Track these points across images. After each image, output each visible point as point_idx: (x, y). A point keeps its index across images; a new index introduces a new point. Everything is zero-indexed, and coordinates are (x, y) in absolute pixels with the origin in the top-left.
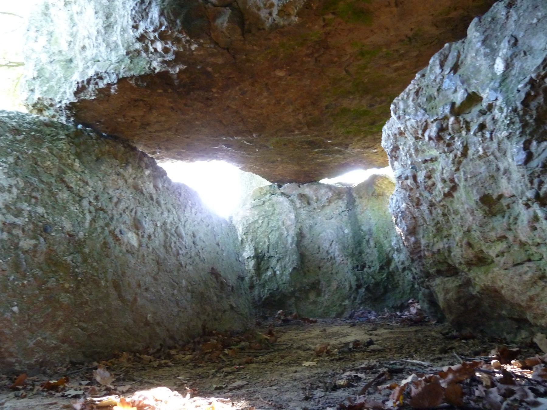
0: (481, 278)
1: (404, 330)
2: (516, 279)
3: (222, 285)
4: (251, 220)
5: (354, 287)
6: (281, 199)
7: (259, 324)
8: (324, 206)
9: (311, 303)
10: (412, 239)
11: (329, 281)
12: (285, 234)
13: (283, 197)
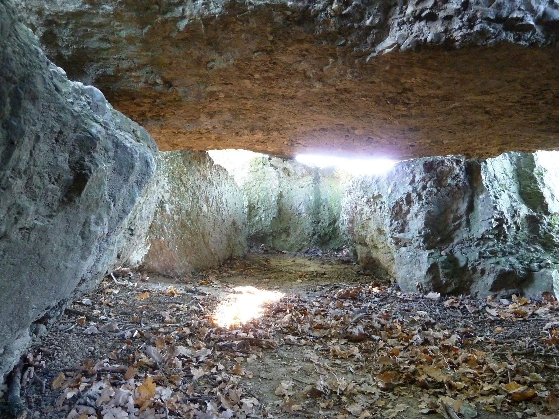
0: (375, 254)
1: (339, 266)
2: (385, 258)
4: (248, 181)
6: (271, 169)
7: (249, 252)
8: (298, 178)
9: (283, 241)
10: (351, 225)
11: (296, 229)
12: (271, 194)
13: (272, 168)
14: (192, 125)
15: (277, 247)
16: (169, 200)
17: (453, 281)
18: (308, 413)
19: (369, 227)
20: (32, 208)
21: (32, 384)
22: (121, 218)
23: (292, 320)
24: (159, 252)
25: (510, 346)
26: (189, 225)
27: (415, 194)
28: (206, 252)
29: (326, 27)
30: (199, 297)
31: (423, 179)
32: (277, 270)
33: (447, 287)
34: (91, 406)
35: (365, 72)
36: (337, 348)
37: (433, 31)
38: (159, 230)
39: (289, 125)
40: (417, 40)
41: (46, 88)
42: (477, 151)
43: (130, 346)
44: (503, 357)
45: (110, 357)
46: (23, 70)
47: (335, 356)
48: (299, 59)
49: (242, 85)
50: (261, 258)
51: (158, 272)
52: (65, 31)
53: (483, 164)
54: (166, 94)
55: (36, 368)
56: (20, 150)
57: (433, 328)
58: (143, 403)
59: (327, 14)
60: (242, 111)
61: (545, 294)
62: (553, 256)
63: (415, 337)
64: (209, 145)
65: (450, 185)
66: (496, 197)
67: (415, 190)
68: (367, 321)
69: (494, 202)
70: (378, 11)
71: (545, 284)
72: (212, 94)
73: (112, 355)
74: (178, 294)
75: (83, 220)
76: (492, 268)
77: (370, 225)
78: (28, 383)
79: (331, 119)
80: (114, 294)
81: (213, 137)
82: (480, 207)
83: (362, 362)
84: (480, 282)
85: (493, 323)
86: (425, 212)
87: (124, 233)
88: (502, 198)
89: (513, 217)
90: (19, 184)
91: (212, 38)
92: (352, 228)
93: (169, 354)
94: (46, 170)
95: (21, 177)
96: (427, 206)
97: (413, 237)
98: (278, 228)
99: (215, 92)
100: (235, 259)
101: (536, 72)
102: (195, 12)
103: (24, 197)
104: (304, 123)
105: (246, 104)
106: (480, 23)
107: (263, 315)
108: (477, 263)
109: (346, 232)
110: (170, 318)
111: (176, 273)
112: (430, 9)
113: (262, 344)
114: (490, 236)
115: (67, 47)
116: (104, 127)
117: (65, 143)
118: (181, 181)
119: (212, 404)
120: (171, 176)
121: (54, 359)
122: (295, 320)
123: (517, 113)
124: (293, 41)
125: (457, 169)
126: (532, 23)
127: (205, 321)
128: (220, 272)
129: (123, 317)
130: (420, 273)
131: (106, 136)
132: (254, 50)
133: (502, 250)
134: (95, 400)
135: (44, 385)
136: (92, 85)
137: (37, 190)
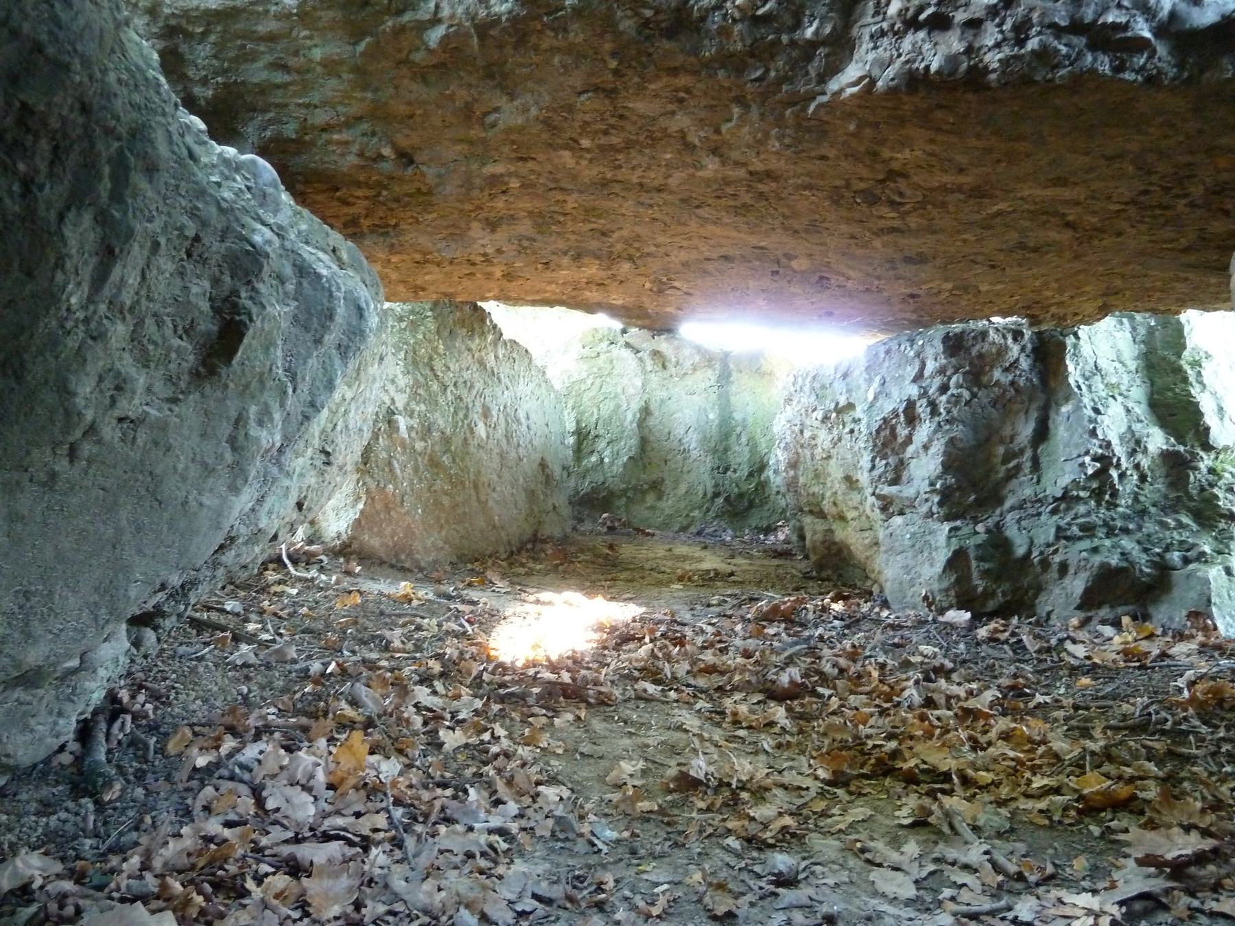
0: (840, 534)
1: (766, 562)
3: (548, 479)
4: (576, 377)
5: (709, 495)
6: (627, 353)
7: (574, 529)
8: (686, 374)
9: (648, 508)
10: (792, 473)
11: (677, 482)
12: (624, 407)
13: (629, 350)
14: (453, 246)
15: (636, 522)
16: (405, 409)
17: (999, 587)
18: (669, 816)
19: (829, 475)
20: (141, 381)
21: (129, 746)
22: (307, 418)
23: (653, 655)
24: (382, 516)
25: (1103, 713)
26: (448, 464)
27: (924, 402)
28: (481, 523)
29: (724, 42)
30: (461, 607)
31: (942, 371)
32: (632, 566)
33: (986, 599)
34: (241, 781)
35: (807, 137)
36: (743, 709)
37: (942, 50)
38: (383, 470)
39: (653, 249)
40: (910, 69)
41: (174, 152)
42: (1053, 310)
43: (319, 688)
44: (1086, 733)
45: (280, 706)
46: (134, 115)
47: (736, 723)
48: (670, 107)
49: (556, 161)
50: (600, 543)
51: (380, 558)
52: (200, 47)
53: (1070, 340)
54: (401, 180)
55: (135, 718)
56: (124, 267)
57: (948, 679)
58: (342, 780)
59: (726, 15)
60: (555, 216)
61: (1194, 615)
62: (1216, 538)
63: (906, 693)
64: (489, 291)
65: (997, 383)
66: (1097, 411)
67: (924, 394)
68: (809, 660)
69: (1090, 421)
70: (831, 10)
71: (1193, 595)
72: (494, 180)
73: (283, 703)
74: (419, 599)
75: (234, 414)
76: (1083, 561)
77: (830, 470)
78: (119, 742)
79: (742, 235)
80: (289, 596)
81: (498, 274)
82: (1061, 431)
83: (792, 735)
84: (1057, 591)
85: (1074, 671)
86: (943, 441)
87: (312, 459)
88: (1110, 412)
89: (1132, 453)
90: (119, 331)
91: (494, 64)
92: (795, 478)
93: (397, 700)
94: (169, 310)
95: (124, 319)
96: (948, 427)
97: (918, 493)
98: (638, 480)
99: (502, 175)
100: (544, 541)
101: (1165, 137)
102: (460, 10)
103: (128, 359)
104: (685, 243)
105: (565, 201)
106: (1039, 33)
107: (595, 645)
108: (1052, 549)
109: (783, 490)
110: (403, 642)
111: (418, 561)
112: (936, 5)
113: (588, 695)
114: (1082, 494)
115: (204, 82)
116: (278, 235)
117: (205, 261)
118: (432, 369)
119: (479, 793)
120: (410, 359)
121: (170, 705)
122: (660, 655)
123: (1133, 227)
124: (659, 70)
125: (1015, 349)
126: (1147, 34)
127: (474, 649)
128: (511, 564)
129: (307, 637)
130: (931, 571)
131: (281, 252)
132: (579, 89)
133: (1106, 524)
134: (251, 771)
135: (152, 747)
136: (257, 154)
137: (151, 347)
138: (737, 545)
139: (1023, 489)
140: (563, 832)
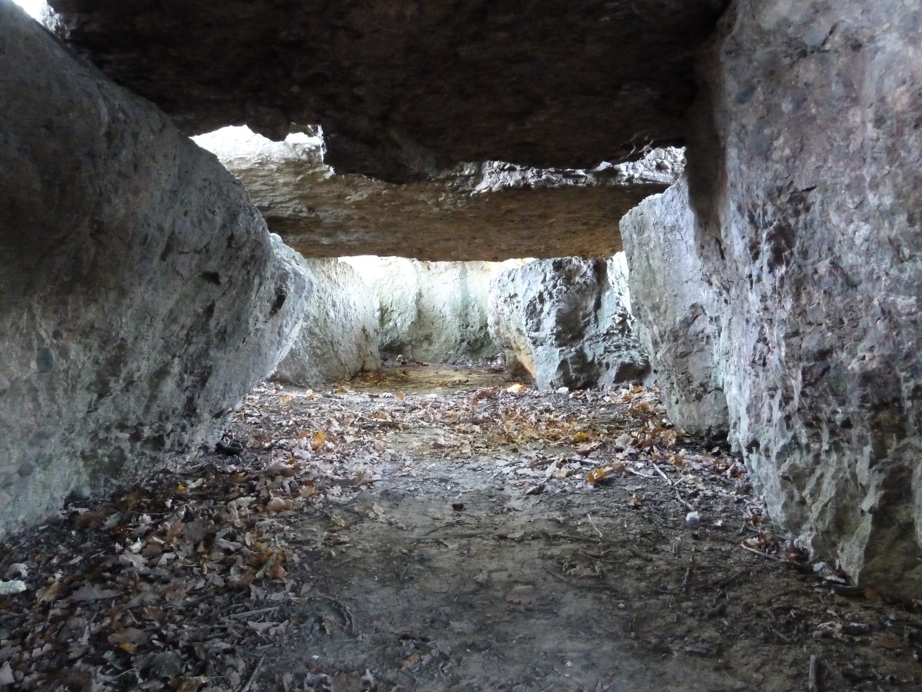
7: (383, 364)
11: (439, 335)
27: (546, 293)
31: (553, 278)
37: (514, 178)
53: (609, 262)
66: (620, 294)
92: (498, 330)
100: (368, 371)
133: (626, 345)
138: (474, 367)
139: (591, 331)
140: (394, 459)
